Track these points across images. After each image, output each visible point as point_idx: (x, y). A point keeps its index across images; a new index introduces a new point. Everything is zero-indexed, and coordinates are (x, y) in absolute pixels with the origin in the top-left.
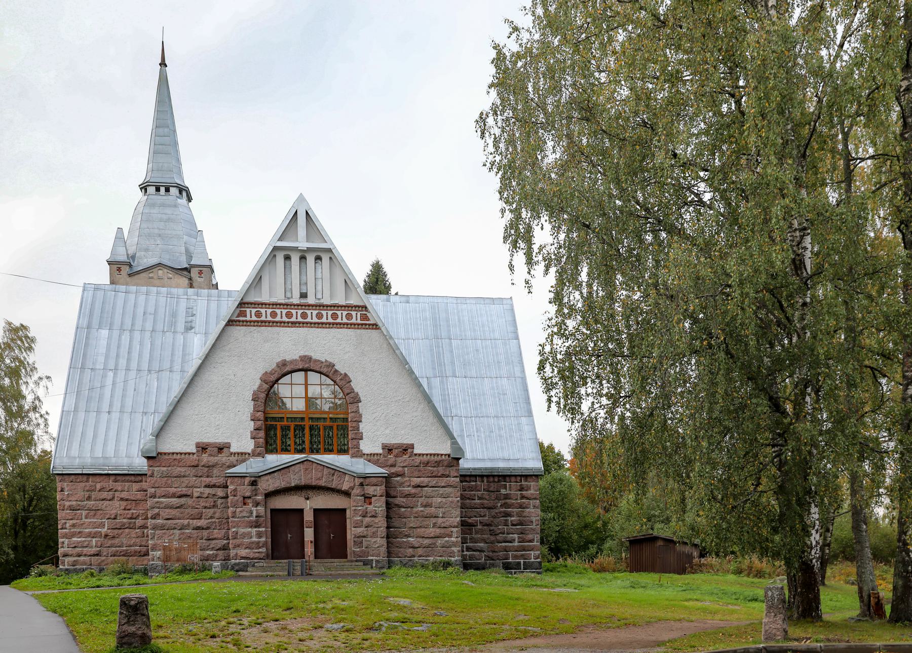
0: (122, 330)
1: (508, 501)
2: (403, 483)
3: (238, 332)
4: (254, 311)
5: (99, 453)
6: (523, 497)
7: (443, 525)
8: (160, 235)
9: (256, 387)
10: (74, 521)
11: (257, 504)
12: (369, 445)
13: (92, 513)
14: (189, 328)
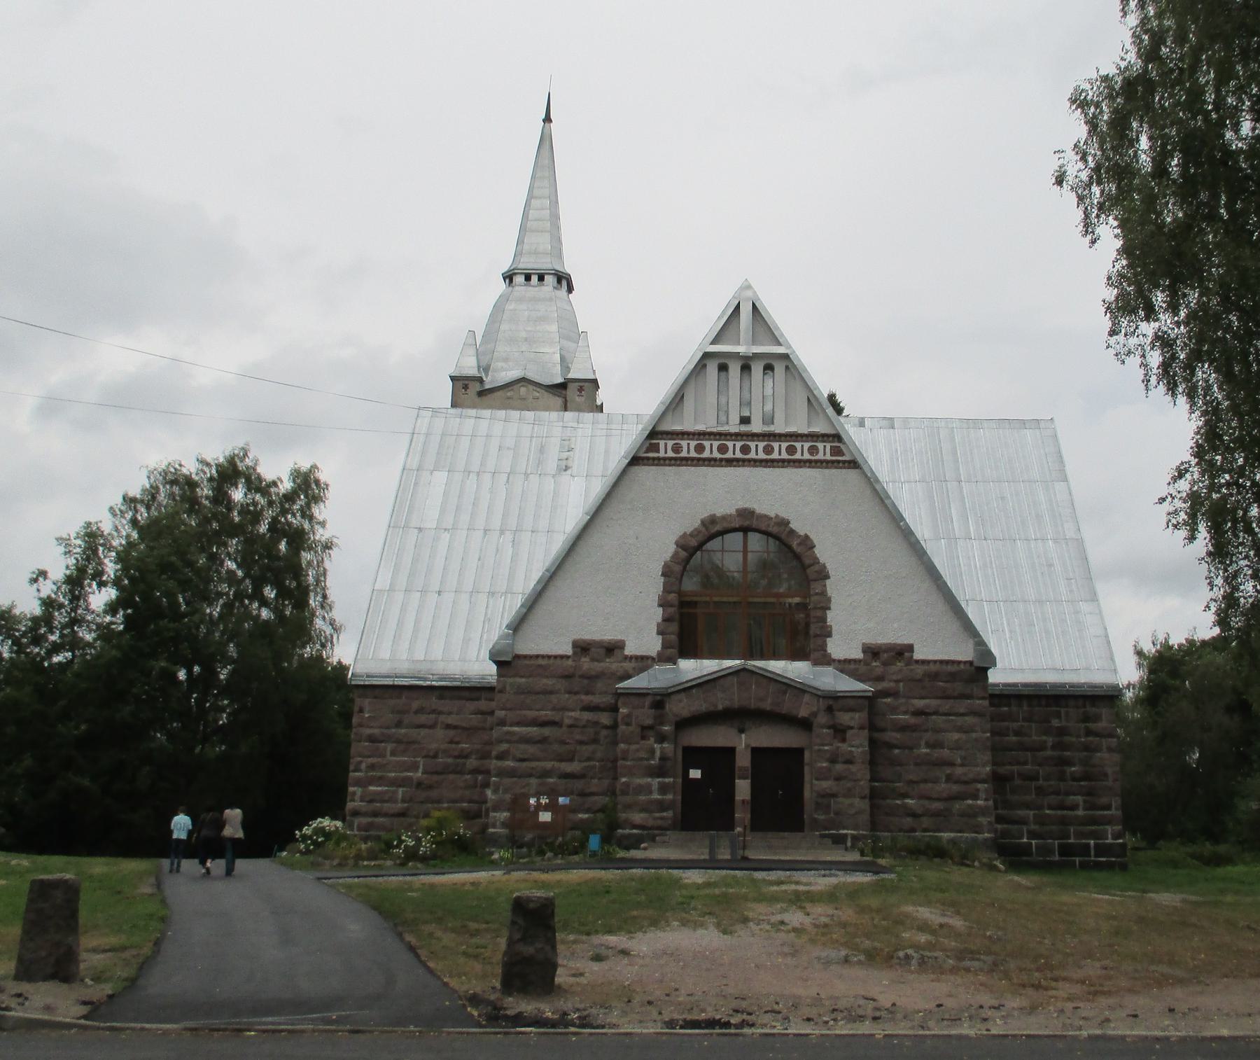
3: (645, 474)
5: (419, 655)
6: (1089, 733)
10: (371, 760)
11: (662, 738)
12: (842, 646)
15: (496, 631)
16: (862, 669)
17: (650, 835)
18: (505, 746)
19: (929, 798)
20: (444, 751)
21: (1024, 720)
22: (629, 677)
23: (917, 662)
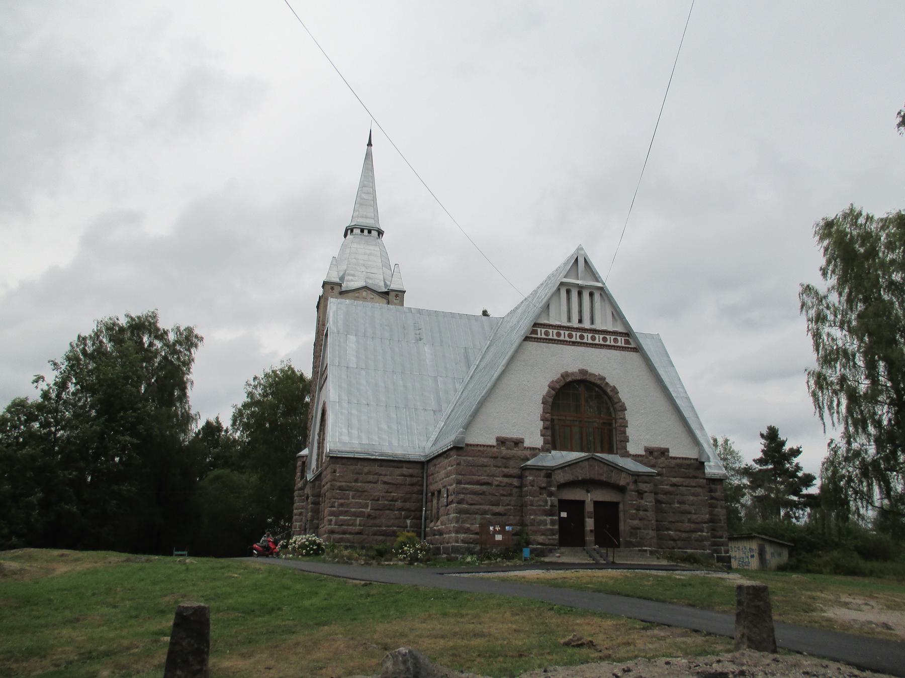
3: (531, 345)
4: (543, 330)
10: (341, 501)
11: (551, 494)
12: (635, 448)
16: (645, 460)
17: (548, 549)
18: (462, 496)
19: (680, 531)
20: (383, 497)
22: (528, 460)
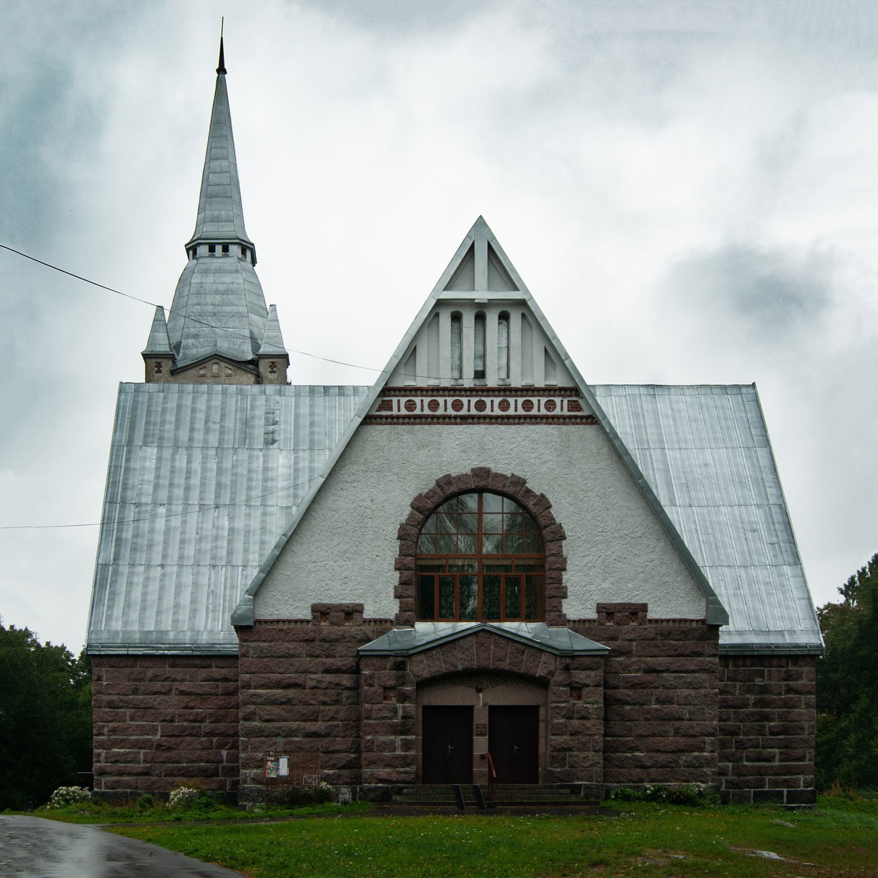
0: (176, 447)
1: (766, 696)
2: (628, 666)
3: (379, 433)
4: (403, 400)
5: (150, 626)
6: (789, 690)
7: (691, 732)
8: (215, 314)
9: (403, 518)
10: (115, 724)
11: (404, 698)
12: (576, 608)
13: (141, 712)
14: (270, 441)
15: (238, 596)
18: (252, 707)
21: (729, 679)
22: (369, 640)
23: (650, 621)
